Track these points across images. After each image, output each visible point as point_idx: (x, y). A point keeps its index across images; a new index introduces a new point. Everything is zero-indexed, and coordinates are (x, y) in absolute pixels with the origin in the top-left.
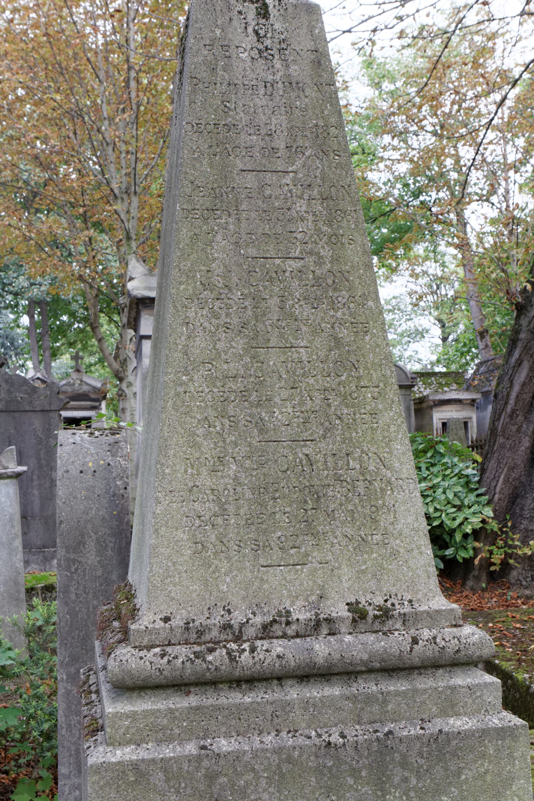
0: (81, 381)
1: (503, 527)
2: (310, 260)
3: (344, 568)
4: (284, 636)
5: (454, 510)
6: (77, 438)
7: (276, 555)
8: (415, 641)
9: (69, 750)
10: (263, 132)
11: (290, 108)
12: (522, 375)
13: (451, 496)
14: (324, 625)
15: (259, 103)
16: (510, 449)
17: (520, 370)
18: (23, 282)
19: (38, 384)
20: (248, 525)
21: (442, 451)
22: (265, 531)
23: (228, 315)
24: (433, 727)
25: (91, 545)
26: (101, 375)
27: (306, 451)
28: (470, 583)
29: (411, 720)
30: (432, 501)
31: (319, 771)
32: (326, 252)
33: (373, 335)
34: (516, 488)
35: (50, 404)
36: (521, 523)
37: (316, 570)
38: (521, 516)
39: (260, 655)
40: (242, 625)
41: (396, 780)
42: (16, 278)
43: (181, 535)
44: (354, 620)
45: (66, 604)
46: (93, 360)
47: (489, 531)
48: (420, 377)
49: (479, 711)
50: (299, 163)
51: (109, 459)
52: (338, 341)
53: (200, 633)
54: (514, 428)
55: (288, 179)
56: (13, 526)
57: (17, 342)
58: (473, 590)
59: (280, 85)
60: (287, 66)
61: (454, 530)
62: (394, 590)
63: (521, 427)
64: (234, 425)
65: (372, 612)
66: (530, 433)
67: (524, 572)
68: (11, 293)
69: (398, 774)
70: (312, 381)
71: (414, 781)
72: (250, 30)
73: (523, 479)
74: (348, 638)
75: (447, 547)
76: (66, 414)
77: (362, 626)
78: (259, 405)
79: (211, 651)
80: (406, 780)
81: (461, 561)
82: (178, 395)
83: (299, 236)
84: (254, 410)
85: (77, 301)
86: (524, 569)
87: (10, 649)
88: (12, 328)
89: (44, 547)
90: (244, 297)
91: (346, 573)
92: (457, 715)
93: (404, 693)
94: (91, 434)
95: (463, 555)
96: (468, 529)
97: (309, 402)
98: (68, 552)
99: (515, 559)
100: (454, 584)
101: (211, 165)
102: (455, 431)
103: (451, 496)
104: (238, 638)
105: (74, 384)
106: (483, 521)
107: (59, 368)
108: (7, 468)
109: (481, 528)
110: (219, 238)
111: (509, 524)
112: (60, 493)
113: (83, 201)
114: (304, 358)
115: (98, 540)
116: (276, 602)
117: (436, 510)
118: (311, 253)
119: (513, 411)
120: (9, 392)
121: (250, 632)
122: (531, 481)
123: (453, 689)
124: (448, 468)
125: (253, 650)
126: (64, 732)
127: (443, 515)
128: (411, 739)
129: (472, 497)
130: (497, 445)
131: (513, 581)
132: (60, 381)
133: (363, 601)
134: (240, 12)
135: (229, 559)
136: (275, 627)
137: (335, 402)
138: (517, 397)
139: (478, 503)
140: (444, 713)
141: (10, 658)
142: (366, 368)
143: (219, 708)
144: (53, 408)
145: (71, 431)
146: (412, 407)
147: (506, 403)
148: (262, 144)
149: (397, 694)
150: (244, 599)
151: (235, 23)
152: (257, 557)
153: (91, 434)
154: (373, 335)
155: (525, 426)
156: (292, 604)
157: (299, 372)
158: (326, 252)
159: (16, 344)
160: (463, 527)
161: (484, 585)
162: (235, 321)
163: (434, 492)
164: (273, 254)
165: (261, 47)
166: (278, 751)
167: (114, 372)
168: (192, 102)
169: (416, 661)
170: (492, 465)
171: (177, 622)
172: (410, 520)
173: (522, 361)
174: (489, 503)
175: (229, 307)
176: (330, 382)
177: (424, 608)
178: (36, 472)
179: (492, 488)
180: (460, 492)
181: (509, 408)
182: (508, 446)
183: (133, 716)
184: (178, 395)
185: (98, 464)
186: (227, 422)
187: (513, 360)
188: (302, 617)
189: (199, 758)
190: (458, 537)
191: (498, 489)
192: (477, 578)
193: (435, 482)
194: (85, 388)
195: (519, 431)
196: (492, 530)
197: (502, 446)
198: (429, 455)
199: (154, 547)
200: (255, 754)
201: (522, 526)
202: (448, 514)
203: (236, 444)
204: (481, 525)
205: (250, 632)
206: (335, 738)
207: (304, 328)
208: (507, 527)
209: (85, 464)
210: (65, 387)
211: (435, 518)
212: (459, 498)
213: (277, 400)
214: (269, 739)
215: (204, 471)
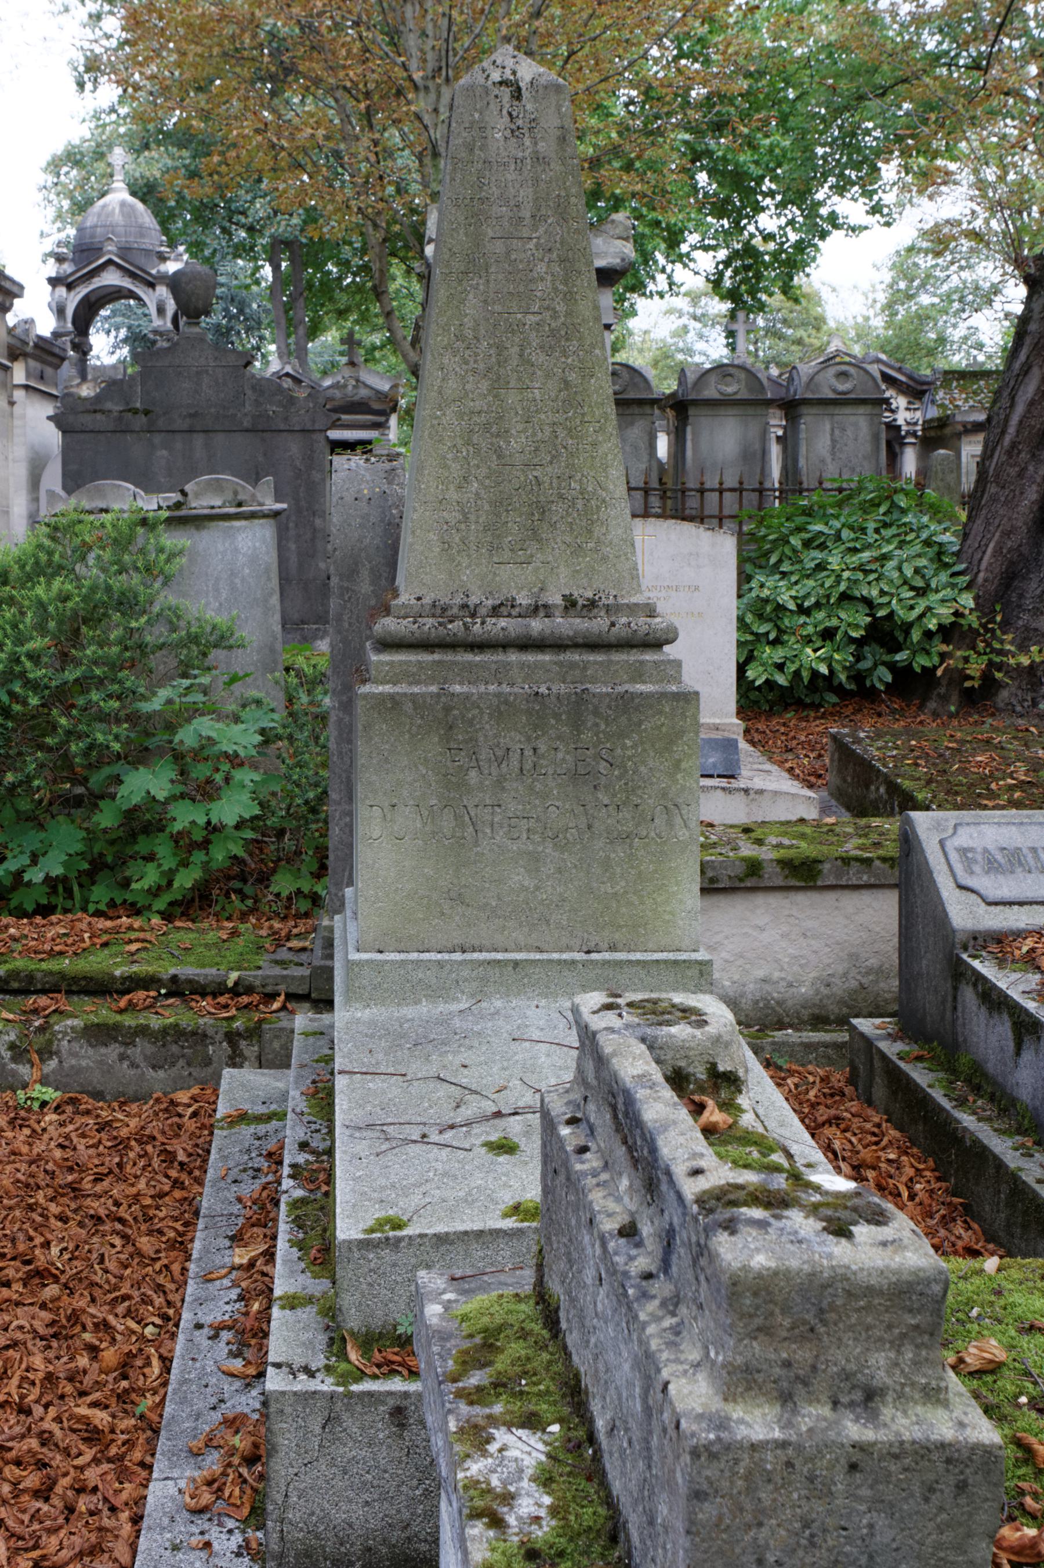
0: (358, 381)
1: (988, 622)
2: (547, 315)
3: (562, 569)
4: (509, 616)
5: (912, 594)
6: (353, 464)
7: (507, 555)
8: (613, 624)
9: (340, 777)
10: (512, 203)
11: (536, 181)
12: (1029, 390)
13: (909, 572)
14: (541, 609)
15: (509, 177)
16: (1006, 503)
17: (1026, 380)
18: (260, 208)
19: (287, 383)
20: (485, 531)
21: (902, 505)
22: (499, 536)
23: (475, 362)
24: (620, 689)
25: (365, 573)
26: (391, 368)
27: (535, 473)
28: (932, 705)
29: (605, 683)
30: (877, 580)
31: (529, 712)
32: (561, 308)
33: (598, 379)
34: (1012, 563)
35: (314, 421)
36: (1019, 618)
37: (538, 568)
38: (1019, 606)
39: (488, 627)
40: (476, 606)
41: (589, 724)
42: (252, 202)
43: (431, 536)
44: (566, 607)
45: (339, 632)
46: (376, 339)
47: (966, 628)
48: (958, 380)
49: (662, 681)
50: (541, 230)
51: (385, 487)
52: (566, 383)
53: (444, 610)
54: (1013, 471)
55: (531, 245)
56: (269, 579)
57: (250, 306)
58: (935, 715)
59: (529, 161)
60: (536, 143)
61: (911, 625)
62: (602, 587)
63: (1024, 469)
64: (478, 451)
65: (581, 602)
66: (1039, 480)
67: (1019, 693)
68: (243, 226)
69: (590, 720)
70: (543, 416)
71: (603, 727)
72: (505, 112)
73: (1025, 550)
74: (559, 620)
75: (899, 649)
76: (335, 434)
77: (572, 612)
78: (498, 436)
79: (451, 622)
80: (597, 725)
81: (918, 670)
82: (433, 426)
83: (539, 294)
84: (494, 440)
85: (350, 243)
86: (1020, 687)
87: (272, 710)
88: (247, 287)
89: (303, 622)
90: (490, 346)
91: (563, 572)
92: (644, 682)
93: (601, 663)
94: (367, 460)
95: (922, 661)
96: (932, 625)
97: (540, 434)
98: (341, 580)
99: (1007, 673)
100: (908, 706)
101: (466, 235)
102: (940, 475)
103: (909, 572)
104: (473, 615)
105: (345, 386)
106: (957, 614)
107: (320, 354)
108: (262, 505)
109: (953, 624)
110: (471, 296)
111: (998, 619)
112: (335, 520)
113: (366, 85)
114: (538, 398)
115: (371, 569)
116: (505, 591)
117: (883, 593)
118: (548, 308)
119: (1014, 445)
120: (257, 403)
121: (483, 611)
122: (1039, 553)
123: (642, 662)
124: (912, 530)
125: (483, 623)
126: (335, 759)
127: (894, 602)
128: (602, 695)
129: (944, 577)
130: (986, 496)
131: (1001, 705)
132: (322, 378)
133: (576, 594)
134: (496, 97)
135: (469, 556)
136: (503, 609)
137: (562, 434)
138: (1021, 422)
139: (953, 586)
140: (633, 680)
141: (273, 720)
142: (590, 406)
143: (455, 663)
144: (317, 427)
145: (346, 457)
146: (883, 436)
147: (1003, 432)
148: (510, 214)
149: (596, 662)
150: (480, 587)
151: (492, 106)
152: (491, 556)
153: (367, 460)
154: (598, 379)
155: (1031, 468)
156: (518, 593)
157: (533, 408)
158: (561, 308)
159: (248, 311)
160: (925, 620)
161: (953, 708)
162: (481, 366)
163: (882, 566)
164: (515, 310)
165: (513, 127)
166: (498, 695)
167: (409, 366)
168: (453, 179)
169: (613, 640)
170: (978, 525)
171: (427, 600)
172: (620, 532)
173: (1030, 367)
174: (969, 587)
175: (476, 355)
176: (559, 417)
177: (626, 601)
178: (293, 518)
179: (975, 562)
180: (925, 567)
181: (1007, 440)
182: (1003, 499)
183: (391, 663)
184: (433, 426)
185: (374, 492)
186: (471, 449)
187: (1017, 366)
188: (524, 602)
189: (438, 695)
190: (916, 635)
191: (984, 565)
192: (944, 699)
193: (884, 551)
194: (363, 392)
195: (1021, 475)
196: (970, 625)
197: (994, 499)
198: (882, 509)
199: (411, 545)
200: (481, 696)
201: (1021, 623)
202: (901, 600)
203: (478, 467)
204: (953, 619)
205: (483, 611)
206: (543, 690)
207: (539, 373)
208: (995, 622)
209: (359, 491)
210: (331, 391)
211: (881, 605)
212: (923, 576)
213: (513, 432)
214: (492, 688)
215: (452, 487)
